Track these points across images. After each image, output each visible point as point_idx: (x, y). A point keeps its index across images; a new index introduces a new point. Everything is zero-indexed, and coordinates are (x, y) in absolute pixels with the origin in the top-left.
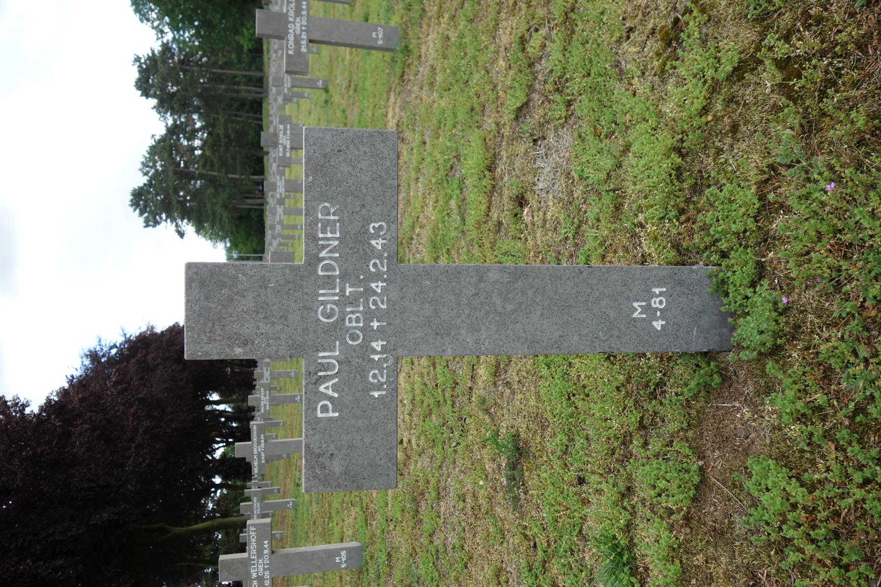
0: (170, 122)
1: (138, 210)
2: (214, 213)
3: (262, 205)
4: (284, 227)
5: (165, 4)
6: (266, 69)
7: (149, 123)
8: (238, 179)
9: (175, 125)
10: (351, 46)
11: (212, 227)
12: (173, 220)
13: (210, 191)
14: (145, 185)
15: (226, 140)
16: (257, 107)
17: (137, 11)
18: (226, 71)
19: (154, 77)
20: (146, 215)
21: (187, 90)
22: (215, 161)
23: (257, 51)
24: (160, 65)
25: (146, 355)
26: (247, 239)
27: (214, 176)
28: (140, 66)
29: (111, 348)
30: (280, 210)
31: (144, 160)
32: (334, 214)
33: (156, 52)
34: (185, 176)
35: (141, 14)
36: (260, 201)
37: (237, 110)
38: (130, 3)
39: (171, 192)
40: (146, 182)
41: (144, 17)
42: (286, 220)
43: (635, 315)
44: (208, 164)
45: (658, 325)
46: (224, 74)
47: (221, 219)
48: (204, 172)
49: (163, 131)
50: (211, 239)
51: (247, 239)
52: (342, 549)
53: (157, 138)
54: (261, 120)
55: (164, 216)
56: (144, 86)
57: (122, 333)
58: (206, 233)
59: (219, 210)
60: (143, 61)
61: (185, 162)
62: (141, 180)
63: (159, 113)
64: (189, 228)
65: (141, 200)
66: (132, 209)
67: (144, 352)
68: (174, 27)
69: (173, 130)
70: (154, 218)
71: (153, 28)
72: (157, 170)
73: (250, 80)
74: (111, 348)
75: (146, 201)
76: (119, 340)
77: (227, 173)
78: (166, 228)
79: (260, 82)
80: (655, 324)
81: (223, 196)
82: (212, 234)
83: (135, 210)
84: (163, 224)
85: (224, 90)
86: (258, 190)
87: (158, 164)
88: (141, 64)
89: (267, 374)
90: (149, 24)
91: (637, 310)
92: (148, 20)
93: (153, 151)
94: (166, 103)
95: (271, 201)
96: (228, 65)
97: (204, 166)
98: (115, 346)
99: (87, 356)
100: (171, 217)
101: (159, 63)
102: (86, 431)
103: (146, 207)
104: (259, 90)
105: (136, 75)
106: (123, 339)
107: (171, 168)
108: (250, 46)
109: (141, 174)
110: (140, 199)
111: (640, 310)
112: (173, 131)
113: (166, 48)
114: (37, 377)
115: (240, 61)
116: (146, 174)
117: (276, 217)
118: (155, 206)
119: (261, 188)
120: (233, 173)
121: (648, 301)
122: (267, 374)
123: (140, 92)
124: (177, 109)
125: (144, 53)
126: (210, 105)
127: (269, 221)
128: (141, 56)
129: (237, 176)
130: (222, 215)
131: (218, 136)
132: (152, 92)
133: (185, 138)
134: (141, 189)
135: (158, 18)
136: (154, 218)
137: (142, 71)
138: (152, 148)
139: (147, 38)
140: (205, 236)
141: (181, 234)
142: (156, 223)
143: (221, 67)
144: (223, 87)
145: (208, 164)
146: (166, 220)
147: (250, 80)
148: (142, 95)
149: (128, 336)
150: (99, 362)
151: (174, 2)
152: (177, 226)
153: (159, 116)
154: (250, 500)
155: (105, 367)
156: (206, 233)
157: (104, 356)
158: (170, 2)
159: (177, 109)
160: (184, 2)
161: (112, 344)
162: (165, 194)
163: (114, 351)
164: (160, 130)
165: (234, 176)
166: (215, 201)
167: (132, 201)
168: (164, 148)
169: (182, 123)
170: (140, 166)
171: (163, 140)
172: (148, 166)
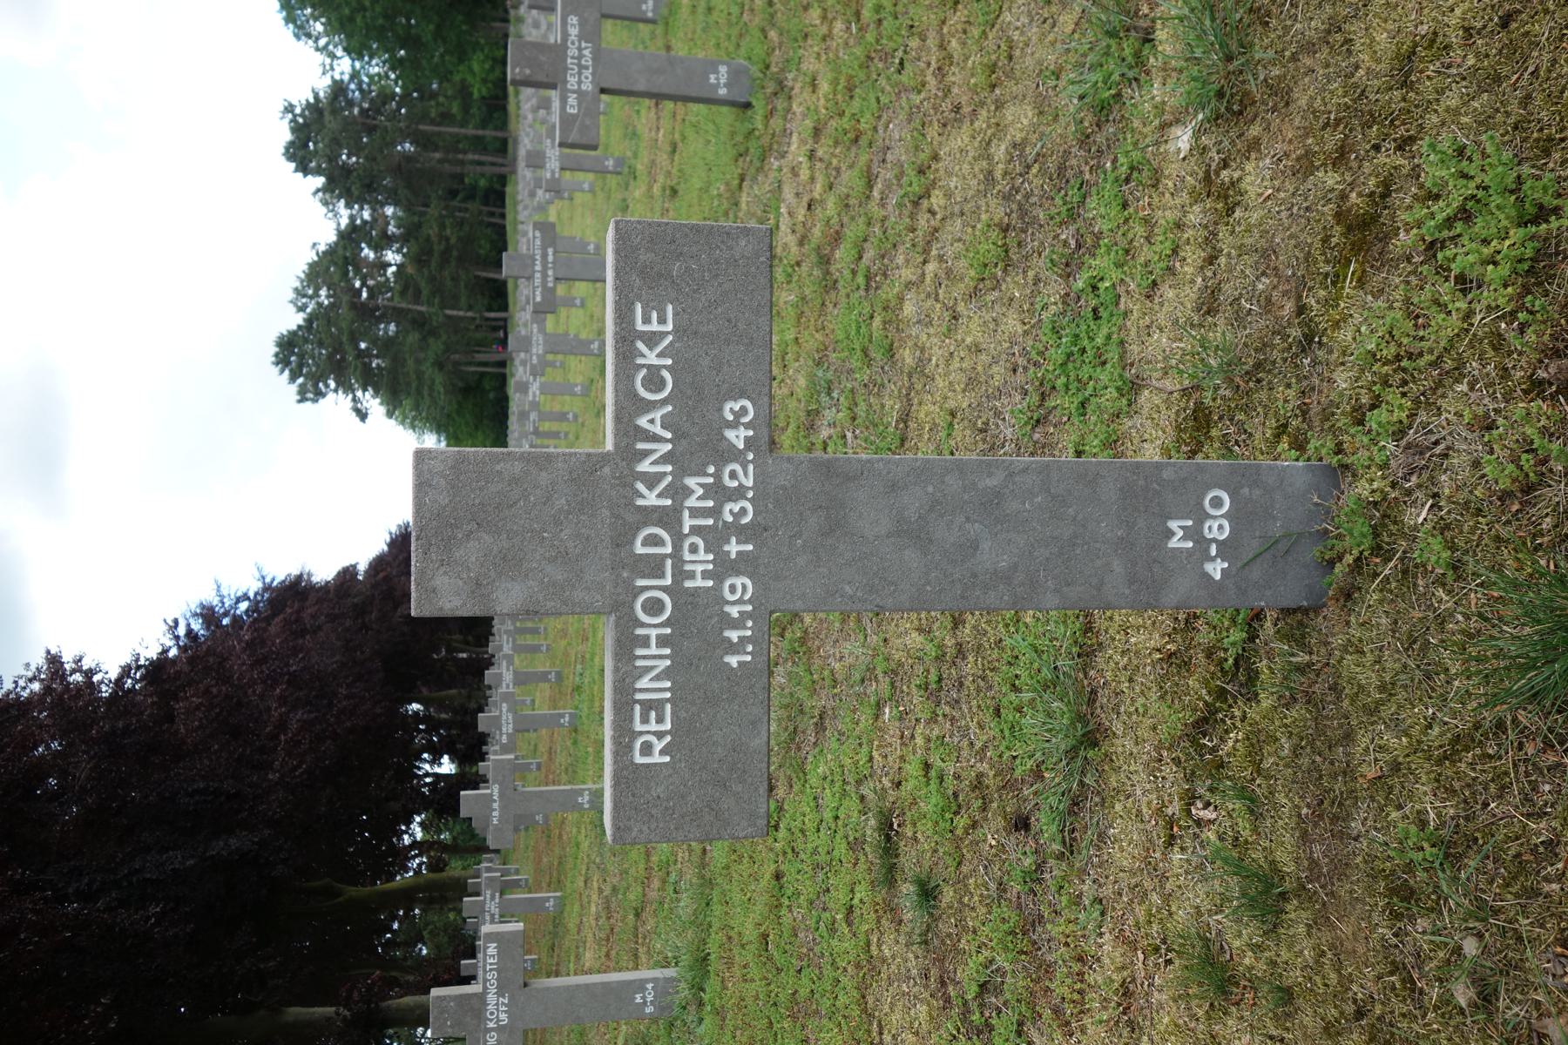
0: (344, 222)
1: (287, 372)
2: (420, 375)
3: (503, 364)
4: (543, 417)
5: (339, 7)
6: (512, 126)
7: (307, 220)
8: (462, 318)
9: (353, 227)
10: (658, 97)
11: (416, 407)
12: (349, 389)
13: (413, 337)
14: (300, 327)
15: (442, 247)
16: (496, 195)
17: (290, 19)
18: (442, 129)
19: (320, 137)
20: (301, 380)
21: (374, 159)
22: (423, 284)
23: (496, 106)
24: (327, 117)
25: (298, 612)
26: (477, 428)
27: (420, 312)
28: (294, 120)
29: (238, 600)
30: (535, 388)
31: (298, 284)
32: (662, 752)
33: (322, 94)
34: (367, 314)
35: (296, 26)
36: (498, 357)
37: (465, 200)
38: (277, 6)
39: (344, 339)
40: (301, 322)
41: (302, 32)
42: (549, 405)
43: (1174, 543)
44: (411, 291)
45: (1216, 569)
46: (439, 133)
47: (431, 389)
48: (404, 305)
49: (332, 237)
50: (413, 427)
51: (477, 428)
52: (647, 981)
53: (322, 248)
54: (503, 216)
55: (332, 384)
56: (300, 154)
57: (257, 575)
58: (405, 417)
59: (428, 370)
60: (298, 111)
61: (370, 290)
62: (293, 320)
63: (325, 203)
64: (374, 404)
65: (293, 353)
66: (276, 370)
67: (296, 605)
68: (354, 51)
69: (350, 234)
70: (316, 386)
71: (317, 49)
72: (320, 305)
73: (479, 144)
74: (238, 600)
75: (301, 356)
76: (253, 586)
77: (443, 306)
78: (336, 403)
79: (503, 147)
80: (1209, 567)
81: (436, 346)
82: (414, 418)
83: (282, 372)
84: (331, 396)
85: (440, 161)
86: (499, 332)
87: (323, 292)
88: (295, 116)
89: (508, 677)
90: (310, 42)
91: (1173, 534)
92: (309, 36)
93: (315, 274)
94: (340, 185)
95: (519, 373)
96: (446, 117)
97: (403, 293)
98: (245, 597)
99: (195, 615)
100: (345, 386)
101: (326, 114)
102: (197, 708)
103: (301, 365)
104: (500, 160)
105: (288, 136)
106: (260, 585)
107: (345, 298)
108: (484, 92)
109: (293, 309)
110: (290, 351)
111: (1181, 533)
112: (350, 236)
113: (338, 89)
114: (114, 624)
115: (466, 108)
116: (302, 309)
117: (528, 389)
118: (318, 366)
119: (501, 334)
120: (453, 308)
121: (1199, 522)
122: (508, 677)
123: (293, 165)
124: (356, 193)
125: (301, 96)
126: (410, 184)
127: (516, 403)
128: (295, 102)
129: (461, 313)
130: (433, 381)
131: (428, 239)
132: (313, 164)
133: (370, 247)
134: (293, 334)
135: (327, 33)
136: (316, 386)
137: (296, 129)
138: (312, 266)
139: (307, 68)
140: (402, 423)
141: (362, 415)
142: (319, 394)
143: (433, 122)
144: (437, 155)
145: (411, 291)
146: (336, 391)
147: (479, 144)
148: (296, 170)
149: (268, 580)
150: (219, 625)
151: (354, 4)
152: (354, 400)
153: (324, 210)
154: (478, 894)
155: (228, 634)
156: (405, 417)
157: (226, 614)
158: (347, 4)
159: (356, 193)
160: (372, 4)
161: (240, 594)
162: (333, 346)
163: (244, 606)
164: (327, 234)
165: (454, 313)
166: (422, 355)
167: (276, 355)
168: (334, 266)
169: (365, 222)
170: (292, 295)
171: (331, 252)
172: (304, 296)
